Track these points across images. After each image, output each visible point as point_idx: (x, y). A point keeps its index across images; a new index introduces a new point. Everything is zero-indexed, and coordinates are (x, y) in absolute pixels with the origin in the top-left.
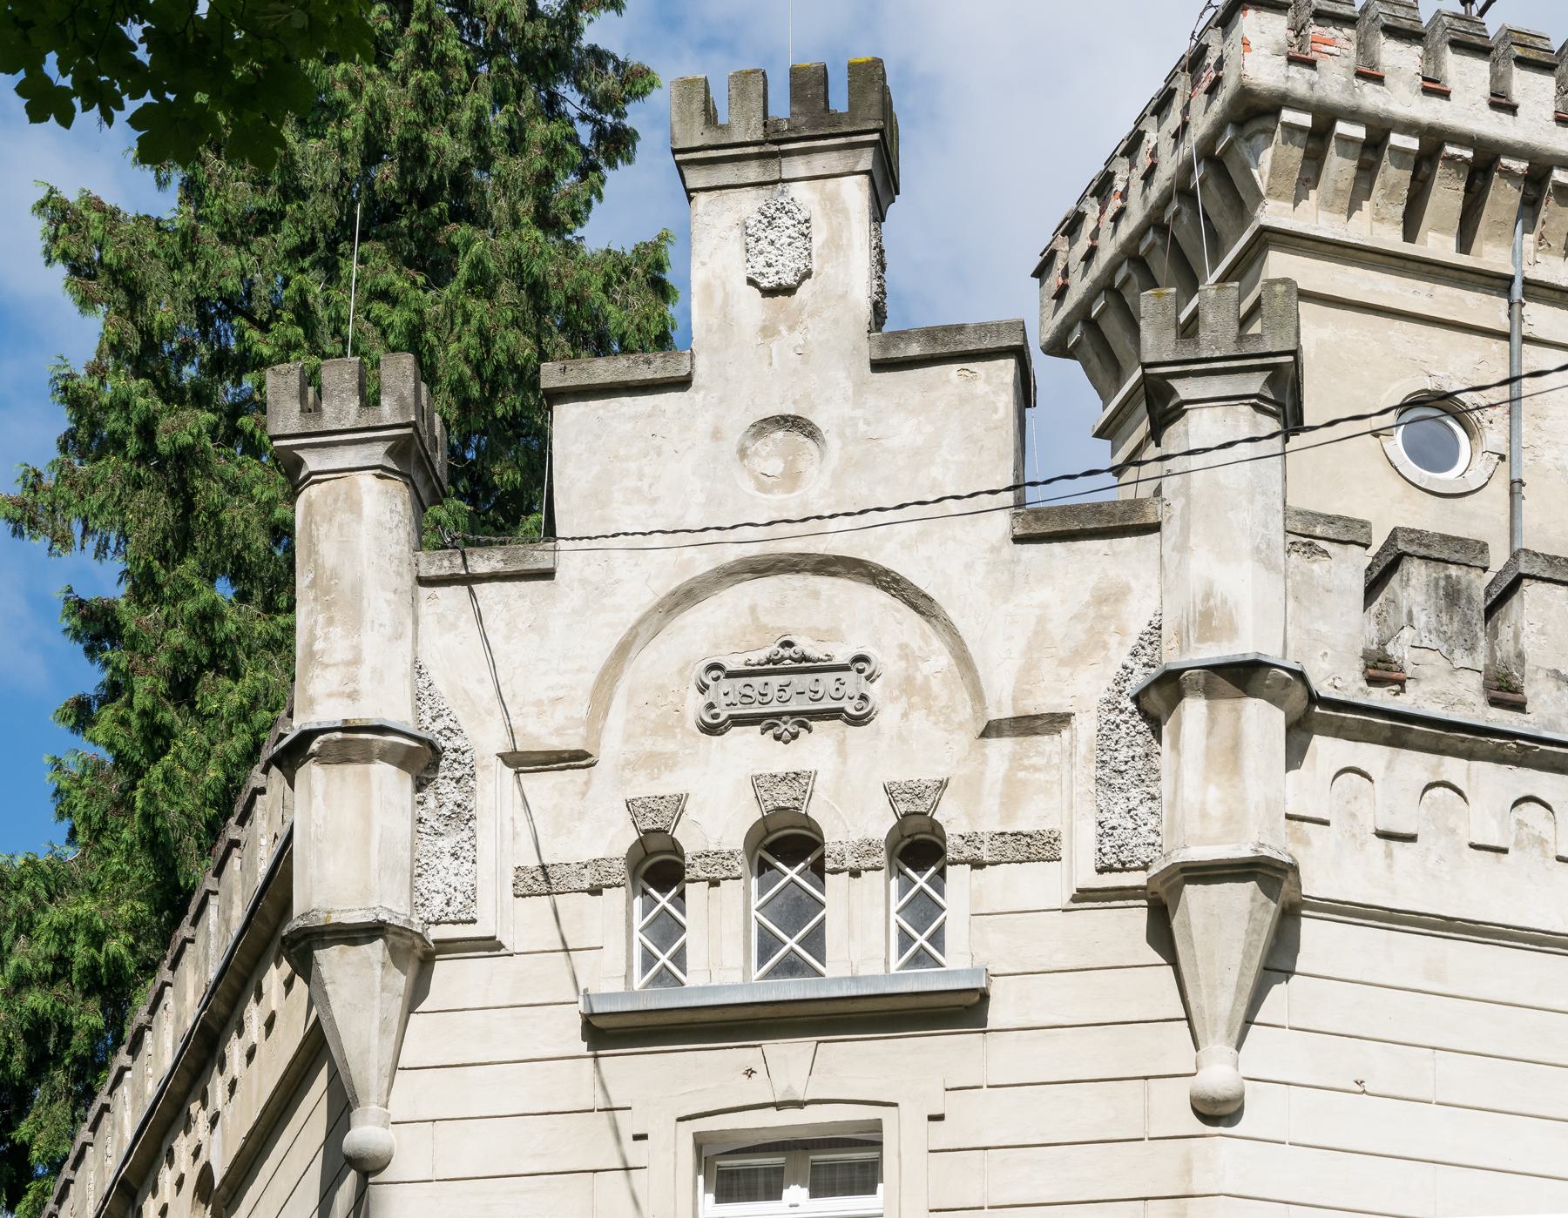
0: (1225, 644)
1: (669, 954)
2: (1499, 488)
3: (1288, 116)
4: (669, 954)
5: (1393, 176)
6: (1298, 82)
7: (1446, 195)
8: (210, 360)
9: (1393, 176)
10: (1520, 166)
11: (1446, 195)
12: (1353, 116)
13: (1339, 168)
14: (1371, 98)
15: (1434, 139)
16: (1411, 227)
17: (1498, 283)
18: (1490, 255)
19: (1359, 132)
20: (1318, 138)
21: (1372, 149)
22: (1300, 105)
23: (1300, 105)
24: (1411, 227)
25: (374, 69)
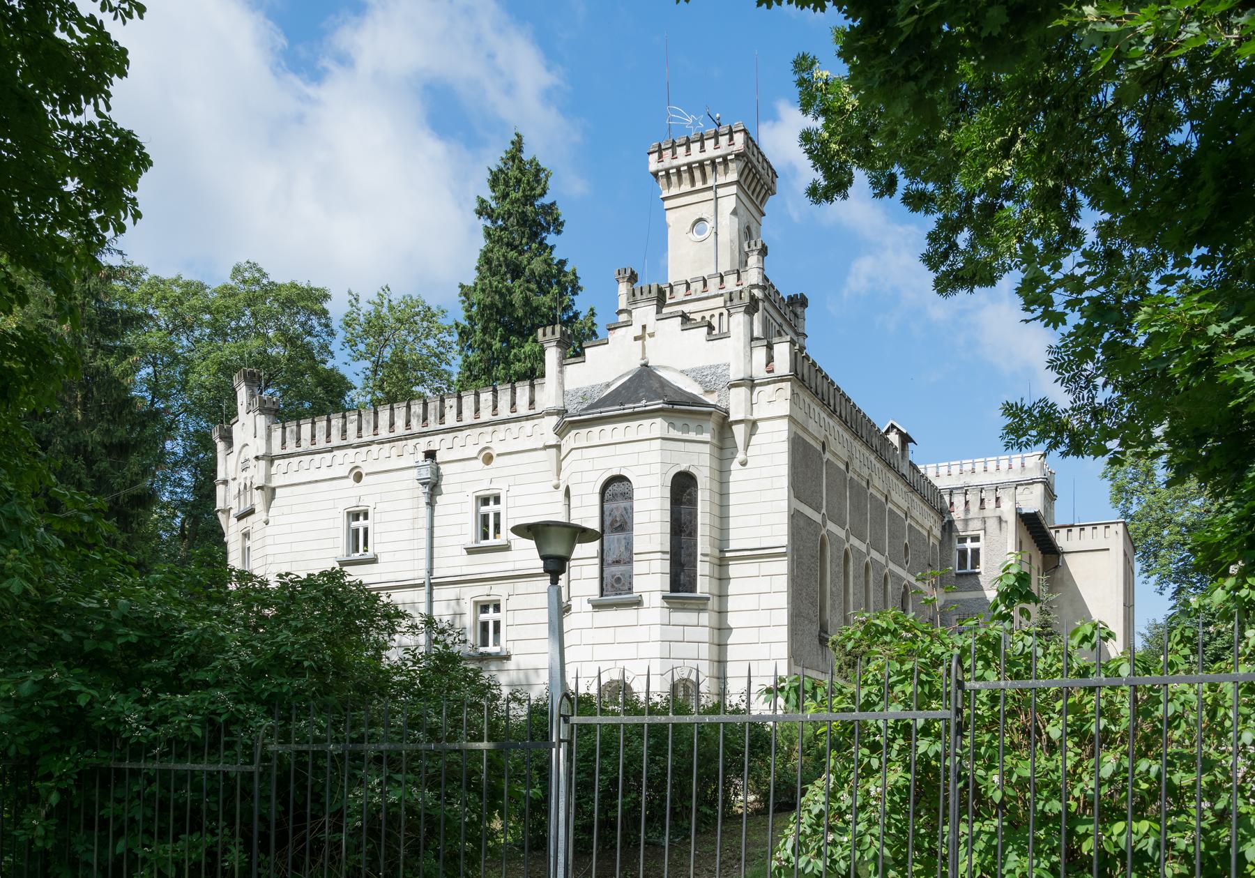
0: (707, 493)
1: (227, 739)
2: (713, 235)
3: (660, 174)
4: (227, 739)
5: (686, 176)
6: (660, 166)
7: (697, 174)
8: (58, 805)
9: (686, 176)
10: (708, 162)
11: (697, 174)
12: (672, 168)
13: (674, 179)
14: (676, 163)
15: (689, 165)
16: (693, 182)
17: (711, 188)
18: (710, 183)
19: (721, 160)
20: (668, 175)
21: (679, 172)
22: (662, 171)
23: (662, 171)
24: (693, 182)
25: (933, 763)
